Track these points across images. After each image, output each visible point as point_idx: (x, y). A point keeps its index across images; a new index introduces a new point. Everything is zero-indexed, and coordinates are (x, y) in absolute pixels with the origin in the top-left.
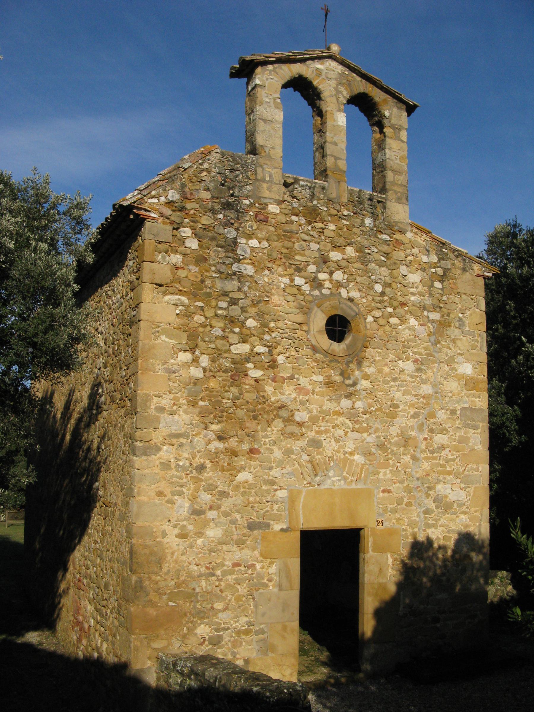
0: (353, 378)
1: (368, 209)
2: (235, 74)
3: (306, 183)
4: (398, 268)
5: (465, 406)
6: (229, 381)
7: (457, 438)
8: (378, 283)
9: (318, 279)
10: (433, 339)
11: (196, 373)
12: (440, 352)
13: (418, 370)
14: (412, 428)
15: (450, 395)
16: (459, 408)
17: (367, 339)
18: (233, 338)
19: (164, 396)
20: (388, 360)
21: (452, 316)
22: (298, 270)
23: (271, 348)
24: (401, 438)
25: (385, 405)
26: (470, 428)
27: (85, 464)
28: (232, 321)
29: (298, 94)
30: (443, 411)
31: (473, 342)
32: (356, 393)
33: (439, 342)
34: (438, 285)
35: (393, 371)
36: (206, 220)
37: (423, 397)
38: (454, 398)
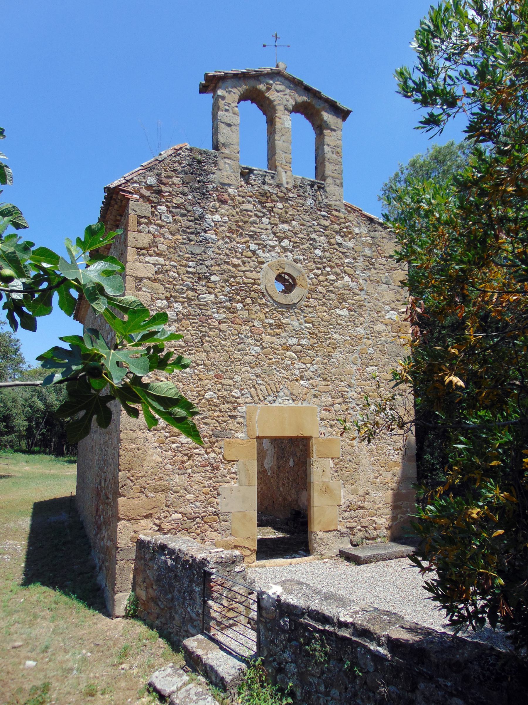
1: (310, 193)
2: (203, 89)
27: (476, 545)
29: (254, 105)
36: (178, 200)
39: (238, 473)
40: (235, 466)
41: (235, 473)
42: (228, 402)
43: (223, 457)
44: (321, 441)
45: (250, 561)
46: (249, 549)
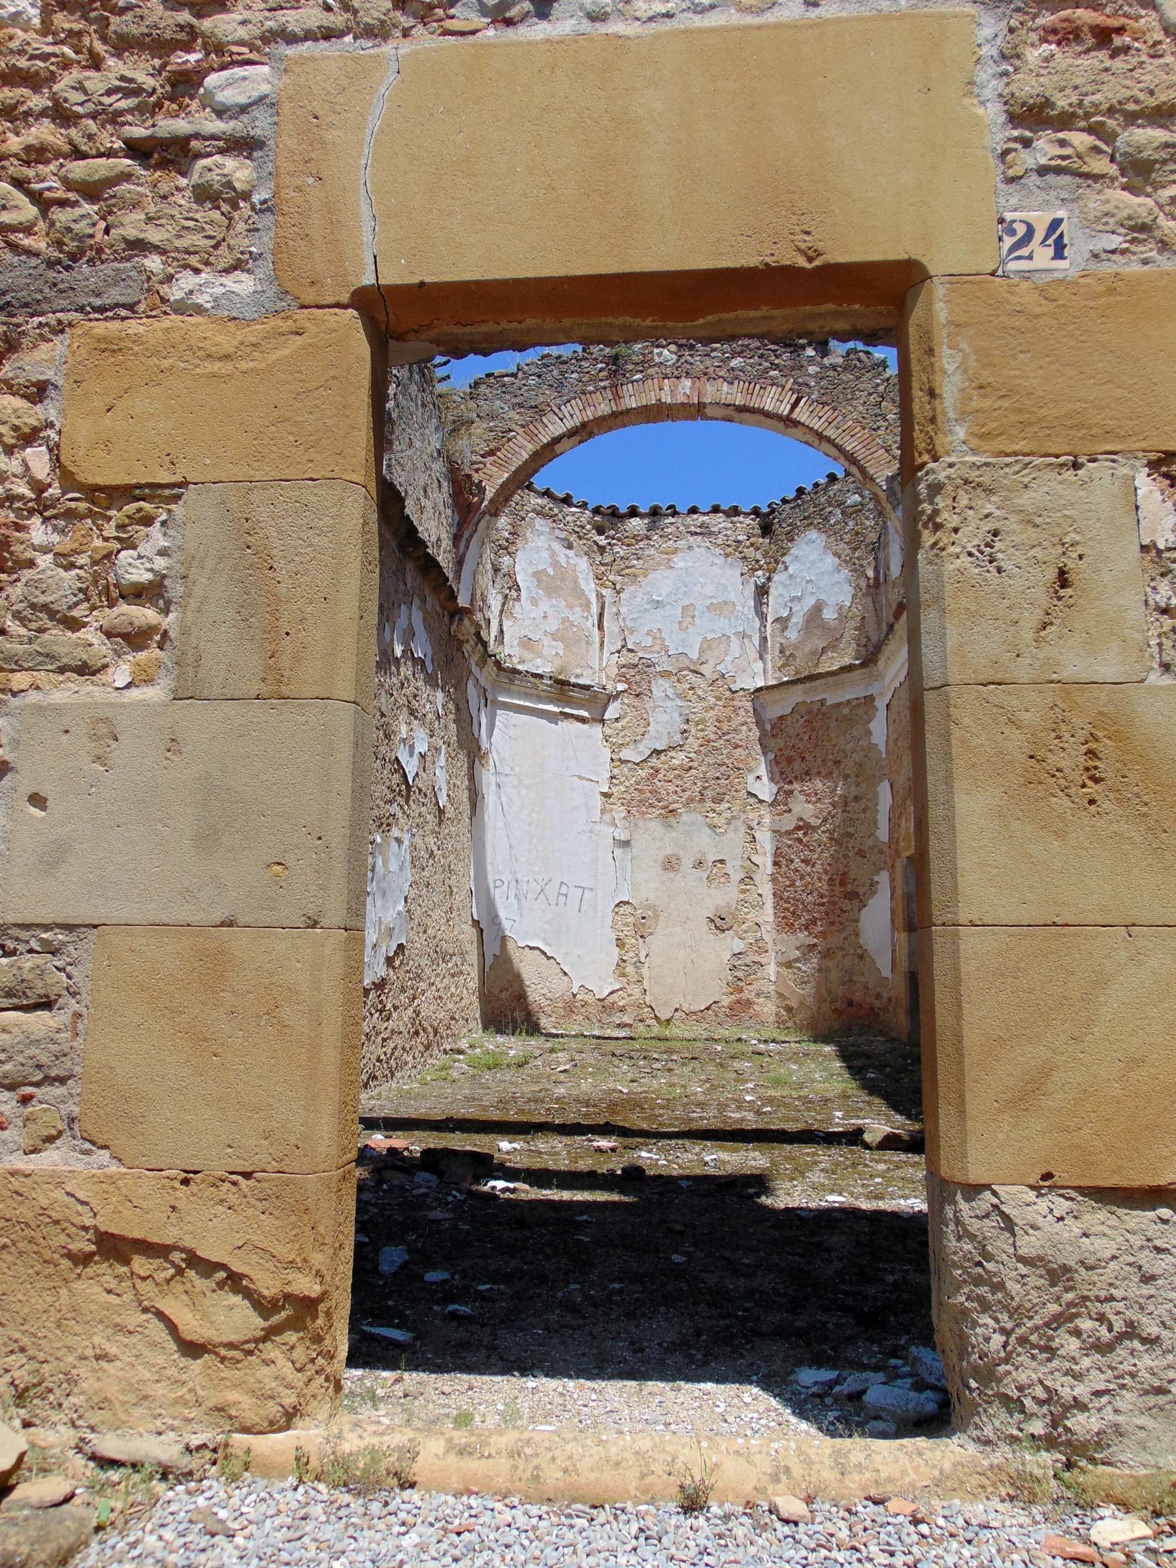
39: (175, 589)
40: (156, 537)
41: (149, 593)
42: (123, 45)
43: (56, 461)
44: (1026, 296)
45: (247, 1407)
46: (235, 1282)
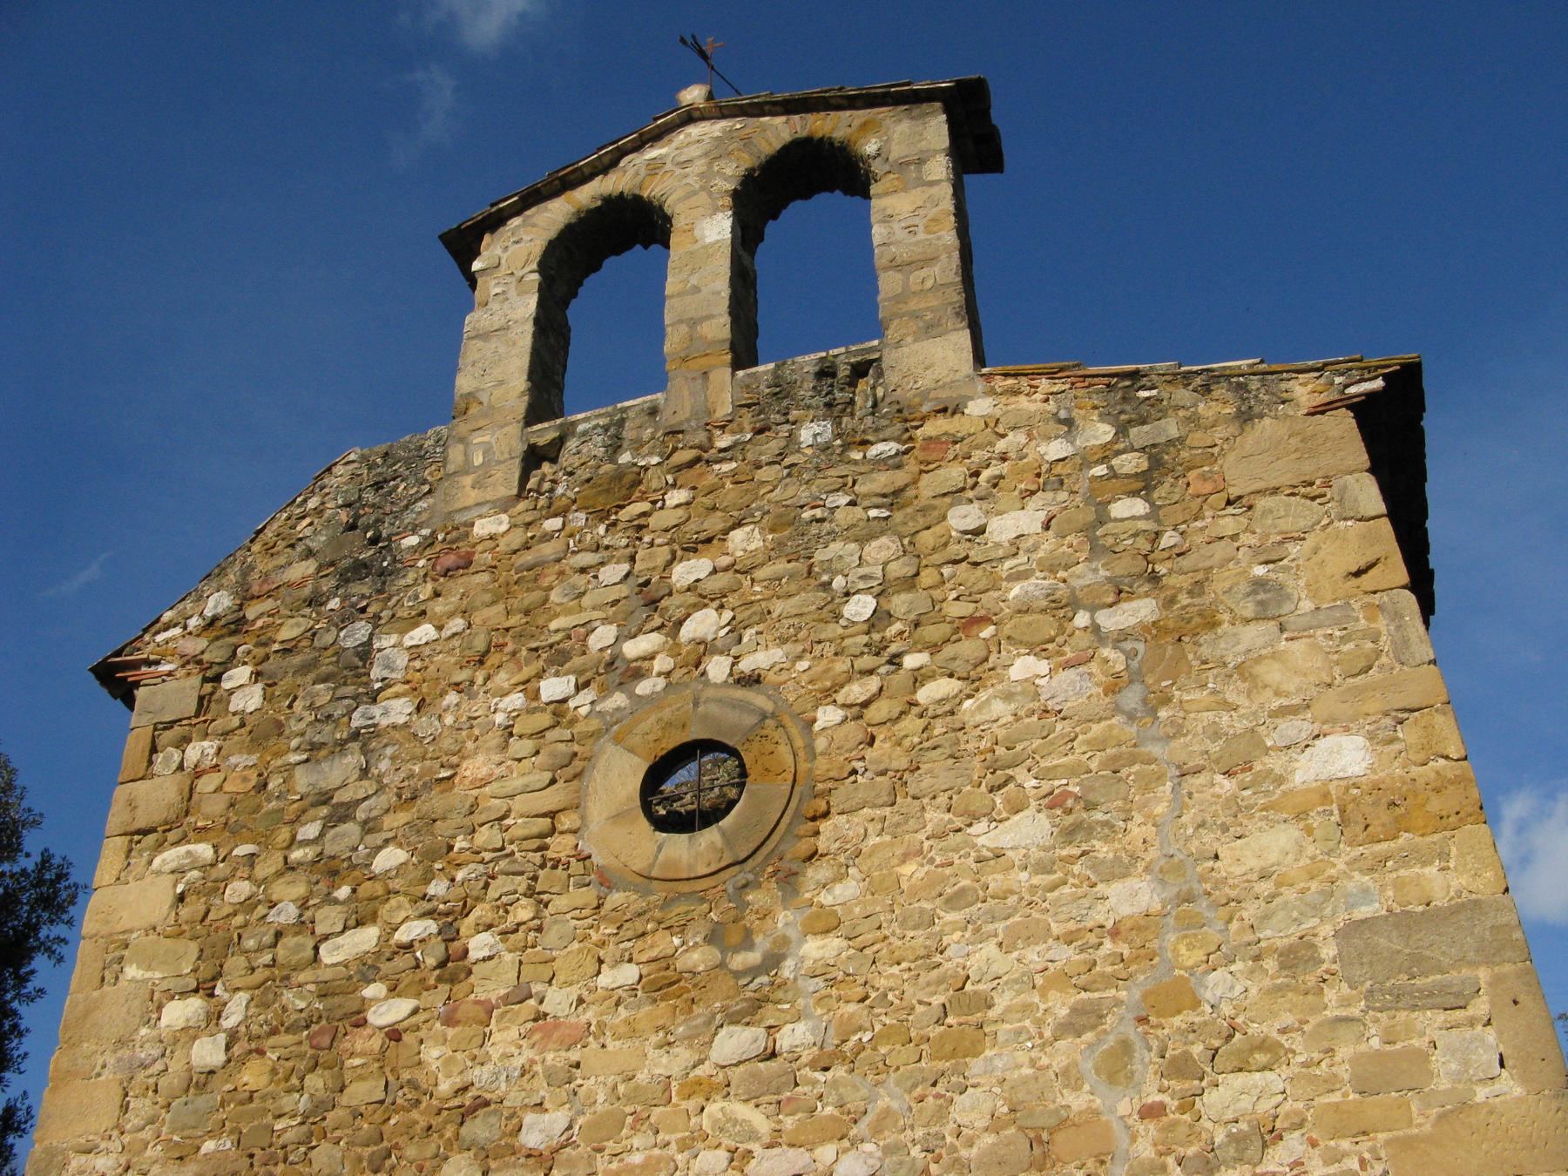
0: (762, 943)
3: (594, 423)
4: (944, 517)
5: (1363, 912)
6: (301, 1056)
7: (1344, 1071)
8: (857, 592)
9: (624, 659)
10: (1131, 698)
11: (208, 1052)
12: (1179, 733)
13: (1069, 834)
14: (1070, 1077)
15: (1265, 888)
16: (1327, 930)
17: (820, 786)
18: (329, 918)
19: (103, 1145)
20: (921, 836)
21: (1218, 586)
22: (558, 658)
23: (450, 921)
24: (1012, 1130)
25: (920, 1009)
26: (1414, 1008)
28: (330, 869)
30: (1238, 966)
31: (1350, 646)
32: (780, 994)
33: (1166, 700)
34: (1128, 508)
35: (948, 871)
37: (1115, 933)
38: (1289, 894)
